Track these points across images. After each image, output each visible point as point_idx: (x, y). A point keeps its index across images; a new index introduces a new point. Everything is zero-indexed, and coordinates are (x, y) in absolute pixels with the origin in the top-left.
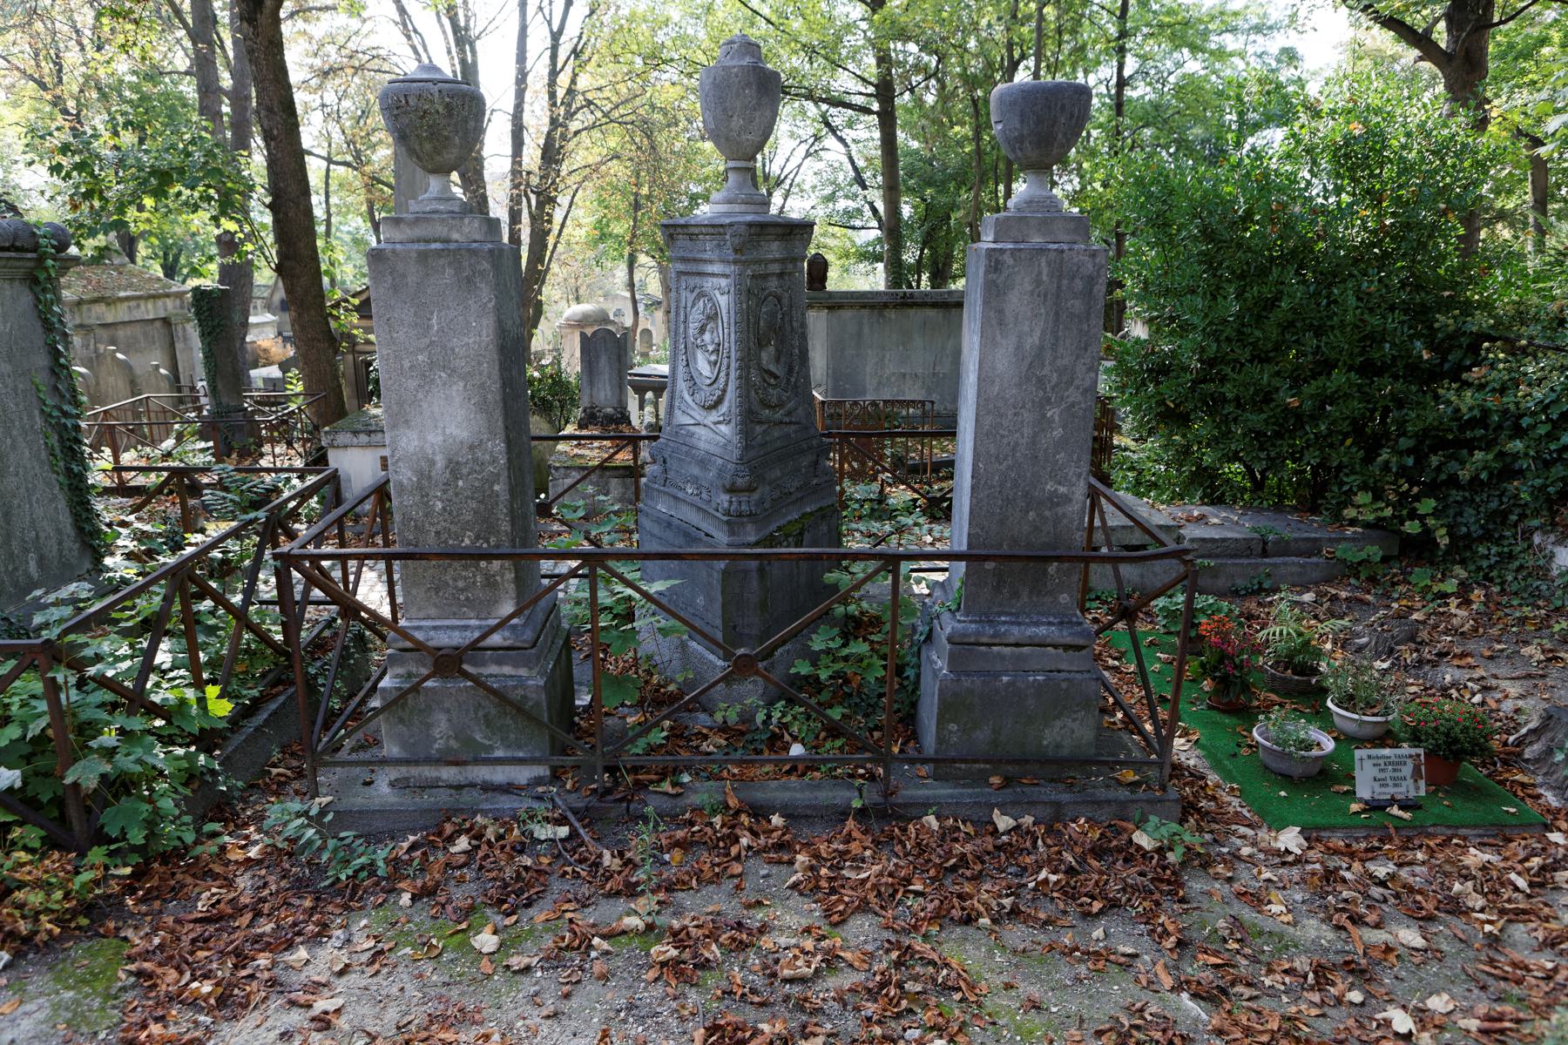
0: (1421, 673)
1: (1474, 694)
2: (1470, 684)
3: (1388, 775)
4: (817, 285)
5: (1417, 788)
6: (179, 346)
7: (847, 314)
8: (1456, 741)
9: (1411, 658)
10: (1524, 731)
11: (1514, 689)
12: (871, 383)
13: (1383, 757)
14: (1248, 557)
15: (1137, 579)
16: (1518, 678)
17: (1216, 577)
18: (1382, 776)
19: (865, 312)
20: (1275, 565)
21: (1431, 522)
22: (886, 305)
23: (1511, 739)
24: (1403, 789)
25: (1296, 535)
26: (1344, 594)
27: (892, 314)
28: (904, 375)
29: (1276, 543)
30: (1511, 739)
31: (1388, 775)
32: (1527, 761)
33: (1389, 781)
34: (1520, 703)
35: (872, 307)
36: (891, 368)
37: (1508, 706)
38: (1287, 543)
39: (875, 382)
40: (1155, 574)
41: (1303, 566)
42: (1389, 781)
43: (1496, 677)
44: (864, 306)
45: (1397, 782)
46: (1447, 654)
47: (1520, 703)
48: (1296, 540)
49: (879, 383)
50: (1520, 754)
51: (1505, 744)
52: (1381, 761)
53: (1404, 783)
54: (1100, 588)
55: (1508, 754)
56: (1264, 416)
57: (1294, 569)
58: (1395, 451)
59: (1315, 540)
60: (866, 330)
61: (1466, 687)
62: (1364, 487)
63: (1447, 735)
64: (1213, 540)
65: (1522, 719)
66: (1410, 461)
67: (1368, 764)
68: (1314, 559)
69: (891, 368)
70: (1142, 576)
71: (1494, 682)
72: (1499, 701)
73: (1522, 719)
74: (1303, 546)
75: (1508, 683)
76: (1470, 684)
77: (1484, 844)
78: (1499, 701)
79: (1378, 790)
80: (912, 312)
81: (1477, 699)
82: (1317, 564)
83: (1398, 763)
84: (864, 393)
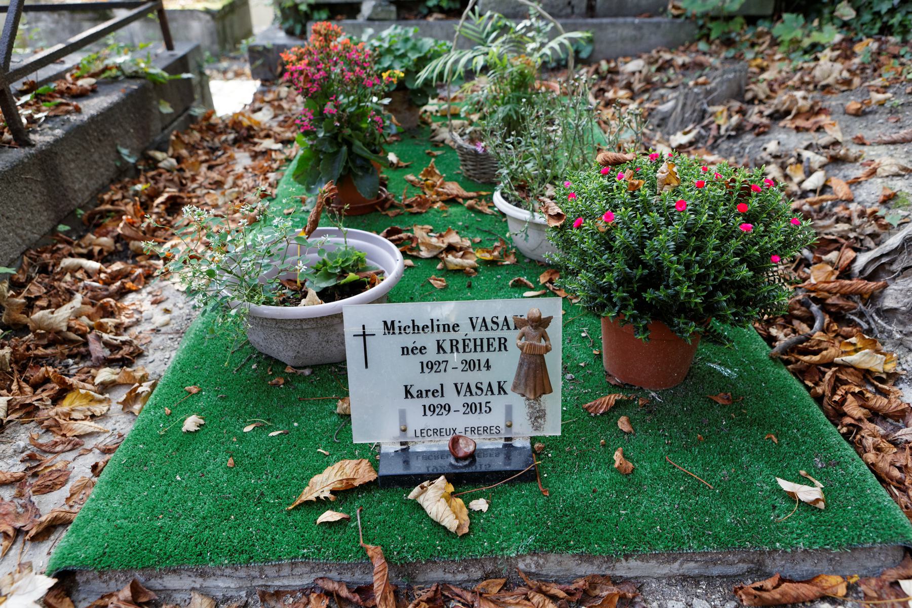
0: (736, 147)
1: (809, 173)
2: (806, 154)
3: (449, 378)
5: (538, 416)
6: (90, 15)
8: (656, 276)
10: (893, 241)
11: (887, 160)
13: (433, 326)
18: (430, 381)
23: (863, 259)
24: (496, 419)
26: (680, 60)
30: (863, 259)
31: (449, 378)
32: (888, 314)
33: (451, 397)
34: (898, 185)
37: (870, 193)
41: (639, 28)
42: (451, 397)
43: (861, 142)
45: (476, 397)
46: (788, 112)
47: (898, 185)
50: (873, 298)
51: (846, 273)
52: (429, 340)
53: (498, 403)
55: (847, 296)
61: (799, 160)
63: (634, 257)
65: (893, 216)
67: (386, 348)
71: (854, 150)
72: (855, 183)
73: (893, 216)
75: (882, 149)
76: (806, 154)
77: (695, 580)
78: (855, 183)
79: (417, 420)
81: (815, 181)
82: (658, 25)
83: (478, 346)
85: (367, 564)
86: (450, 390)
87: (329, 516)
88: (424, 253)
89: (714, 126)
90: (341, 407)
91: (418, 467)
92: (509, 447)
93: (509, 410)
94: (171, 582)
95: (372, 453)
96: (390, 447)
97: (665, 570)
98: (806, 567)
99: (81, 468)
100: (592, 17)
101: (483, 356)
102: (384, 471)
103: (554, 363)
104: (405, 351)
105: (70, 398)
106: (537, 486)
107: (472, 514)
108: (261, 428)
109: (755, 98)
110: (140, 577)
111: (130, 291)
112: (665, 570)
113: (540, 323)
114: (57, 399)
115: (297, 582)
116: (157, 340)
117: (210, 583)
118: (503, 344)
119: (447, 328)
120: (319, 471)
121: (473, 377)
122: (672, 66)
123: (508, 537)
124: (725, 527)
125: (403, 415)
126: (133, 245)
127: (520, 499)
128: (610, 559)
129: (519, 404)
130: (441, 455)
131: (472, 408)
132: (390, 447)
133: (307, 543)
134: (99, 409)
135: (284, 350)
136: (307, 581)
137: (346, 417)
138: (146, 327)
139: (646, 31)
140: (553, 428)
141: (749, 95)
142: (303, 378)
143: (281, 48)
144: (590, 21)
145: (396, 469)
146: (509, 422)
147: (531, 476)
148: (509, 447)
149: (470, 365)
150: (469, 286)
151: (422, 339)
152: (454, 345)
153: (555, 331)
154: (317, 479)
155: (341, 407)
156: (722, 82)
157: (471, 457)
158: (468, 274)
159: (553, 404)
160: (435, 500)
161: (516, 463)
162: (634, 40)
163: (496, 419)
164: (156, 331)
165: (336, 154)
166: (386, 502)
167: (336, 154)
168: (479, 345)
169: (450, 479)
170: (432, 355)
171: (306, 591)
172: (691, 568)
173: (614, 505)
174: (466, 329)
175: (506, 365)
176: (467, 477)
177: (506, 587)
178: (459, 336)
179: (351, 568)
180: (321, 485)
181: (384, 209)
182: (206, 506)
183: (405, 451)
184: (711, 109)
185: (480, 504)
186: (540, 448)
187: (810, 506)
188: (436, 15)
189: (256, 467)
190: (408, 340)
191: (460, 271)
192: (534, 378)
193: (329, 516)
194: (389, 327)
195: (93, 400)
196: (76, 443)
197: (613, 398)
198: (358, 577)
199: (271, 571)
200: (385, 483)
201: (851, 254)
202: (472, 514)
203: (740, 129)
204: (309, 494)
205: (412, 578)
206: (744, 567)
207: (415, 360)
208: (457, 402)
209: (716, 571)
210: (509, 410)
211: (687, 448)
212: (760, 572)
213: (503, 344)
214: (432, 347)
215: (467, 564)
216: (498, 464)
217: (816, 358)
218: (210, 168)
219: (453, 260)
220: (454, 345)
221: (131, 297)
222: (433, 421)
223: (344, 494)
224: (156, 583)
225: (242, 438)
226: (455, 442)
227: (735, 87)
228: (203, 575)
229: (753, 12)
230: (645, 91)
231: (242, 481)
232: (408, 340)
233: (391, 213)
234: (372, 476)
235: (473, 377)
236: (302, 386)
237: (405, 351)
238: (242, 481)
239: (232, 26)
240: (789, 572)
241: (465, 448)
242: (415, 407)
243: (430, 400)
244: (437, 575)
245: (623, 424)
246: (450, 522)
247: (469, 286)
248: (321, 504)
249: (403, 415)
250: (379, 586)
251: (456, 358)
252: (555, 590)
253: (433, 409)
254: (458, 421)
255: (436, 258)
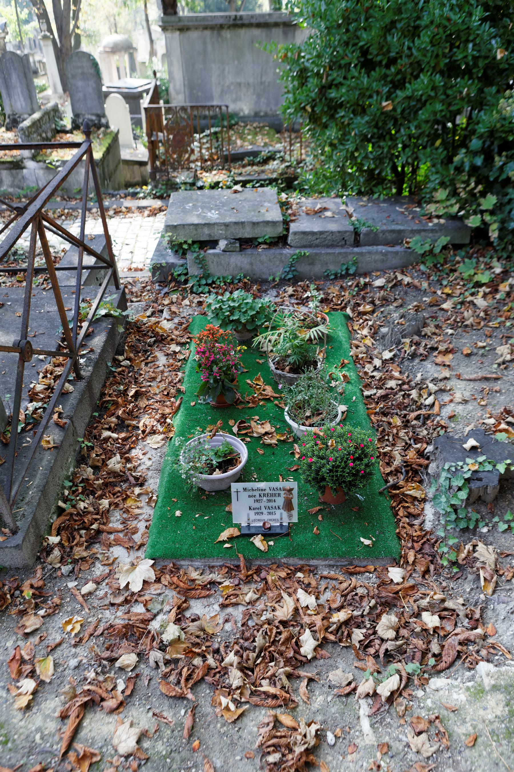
3: (263, 505)
4: (170, 10)
5: (290, 516)
7: (194, 35)
9: (409, 350)
12: (216, 91)
13: (258, 489)
14: (342, 246)
15: (248, 267)
16: (475, 380)
17: (312, 264)
18: (257, 505)
19: (208, 33)
20: (361, 254)
21: (487, 218)
22: (221, 27)
25: (385, 228)
27: (227, 34)
28: (240, 84)
29: (367, 234)
31: (263, 505)
35: (212, 28)
36: (230, 79)
38: (376, 234)
39: (219, 90)
40: (262, 263)
41: (385, 254)
44: (205, 28)
45: (271, 510)
48: (384, 232)
49: (222, 91)
52: (257, 493)
53: (278, 512)
54: (218, 274)
56: (367, 118)
57: (378, 257)
58: (469, 152)
59: (399, 232)
60: (209, 48)
62: (442, 184)
64: (313, 233)
66: (479, 161)
67: (244, 496)
68: (397, 248)
69: (230, 79)
70: (251, 264)
74: (389, 237)
77: (333, 566)
79: (253, 516)
80: (242, 32)
82: (397, 253)
83: (272, 496)
84: (211, 98)
85: (239, 559)
86: (263, 508)
87: (227, 545)
88: (255, 435)
89: (403, 350)
90: (227, 509)
91: (253, 531)
92: (281, 525)
93: (281, 514)
94: (182, 563)
95: (239, 526)
96: (244, 524)
97: (324, 563)
98: (365, 563)
99: (142, 526)
100: (357, 246)
101: (273, 498)
102: (243, 532)
103: (295, 502)
104: (249, 496)
105: (129, 500)
106: (289, 538)
107: (269, 546)
108: (201, 516)
109: (426, 335)
110: (174, 561)
111: (133, 448)
112: (324, 563)
113: (291, 490)
114: (124, 500)
115: (218, 564)
116: (150, 473)
117: (193, 563)
118: (279, 495)
119: (262, 490)
120: (222, 531)
121: (270, 504)
122: (401, 284)
123: (279, 552)
124: (342, 552)
125: (248, 515)
126: (127, 422)
127: (284, 541)
128: (308, 559)
129: (285, 514)
130: (260, 527)
131: (270, 513)
132: (244, 524)
133: (221, 553)
134: (139, 504)
135: (207, 487)
136: (221, 563)
137: (230, 513)
138: (143, 467)
139: (389, 256)
140: (295, 520)
141: (423, 333)
142: (212, 496)
143: (173, 266)
144: (356, 250)
145: (247, 532)
146: (279, 518)
147: (288, 535)
148: (281, 525)
149: (269, 501)
150: (273, 454)
151: (254, 493)
152: (264, 495)
153: (295, 492)
154: (222, 534)
155: (227, 509)
156: (409, 326)
157: (270, 528)
158: (273, 447)
159: (295, 513)
160: (258, 542)
161: (284, 531)
162: (383, 261)
163: (277, 516)
164: (148, 469)
165: (216, 388)
166: (243, 542)
167: (216, 388)
168: (272, 495)
169: (262, 535)
170: (257, 497)
171: (221, 566)
172: (332, 563)
173: (311, 544)
174: (268, 491)
175: (280, 501)
176: (268, 534)
177: (278, 567)
178: (266, 492)
179: (234, 560)
180: (224, 535)
181: (237, 405)
182: (189, 541)
183: (249, 526)
184: (403, 340)
185: (271, 543)
186: (290, 526)
187: (368, 546)
188: (263, 246)
189: (202, 530)
190: (251, 493)
191: (270, 445)
192: (288, 506)
193: (227, 545)
194: (245, 489)
195: (136, 501)
196: (136, 517)
197: (318, 508)
198: (236, 563)
199: (211, 561)
200: (243, 536)
201: (425, 445)
202: (269, 546)
203: (414, 356)
204: (221, 539)
205: (251, 564)
206: (347, 563)
207: (252, 499)
208: (265, 511)
209: (339, 564)
210: (281, 514)
211: (339, 526)
212: (351, 564)
213: (279, 495)
214: (258, 496)
215: (267, 560)
216: (278, 531)
217: (398, 492)
218: (146, 364)
219: (268, 440)
220: (264, 495)
221: (133, 451)
222: (258, 517)
223: (231, 539)
224: (178, 563)
225: (196, 519)
226: (264, 524)
227: (416, 329)
228: (192, 561)
229: (457, 242)
230: (382, 306)
231: (199, 534)
232: (251, 493)
233: (240, 407)
234: (239, 534)
235: (270, 504)
236: (212, 499)
237: (249, 496)
238: (199, 534)
239: (108, 166)
240: (360, 564)
241: (268, 526)
242: (252, 513)
243: (257, 511)
244: (258, 563)
245: (320, 518)
246: (262, 548)
247: (273, 454)
248: (224, 542)
249: (248, 515)
250: (242, 565)
251: (265, 499)
252: (292, 568)
253: (258, 513)
254: (266, 517)
255: (260, 438)
